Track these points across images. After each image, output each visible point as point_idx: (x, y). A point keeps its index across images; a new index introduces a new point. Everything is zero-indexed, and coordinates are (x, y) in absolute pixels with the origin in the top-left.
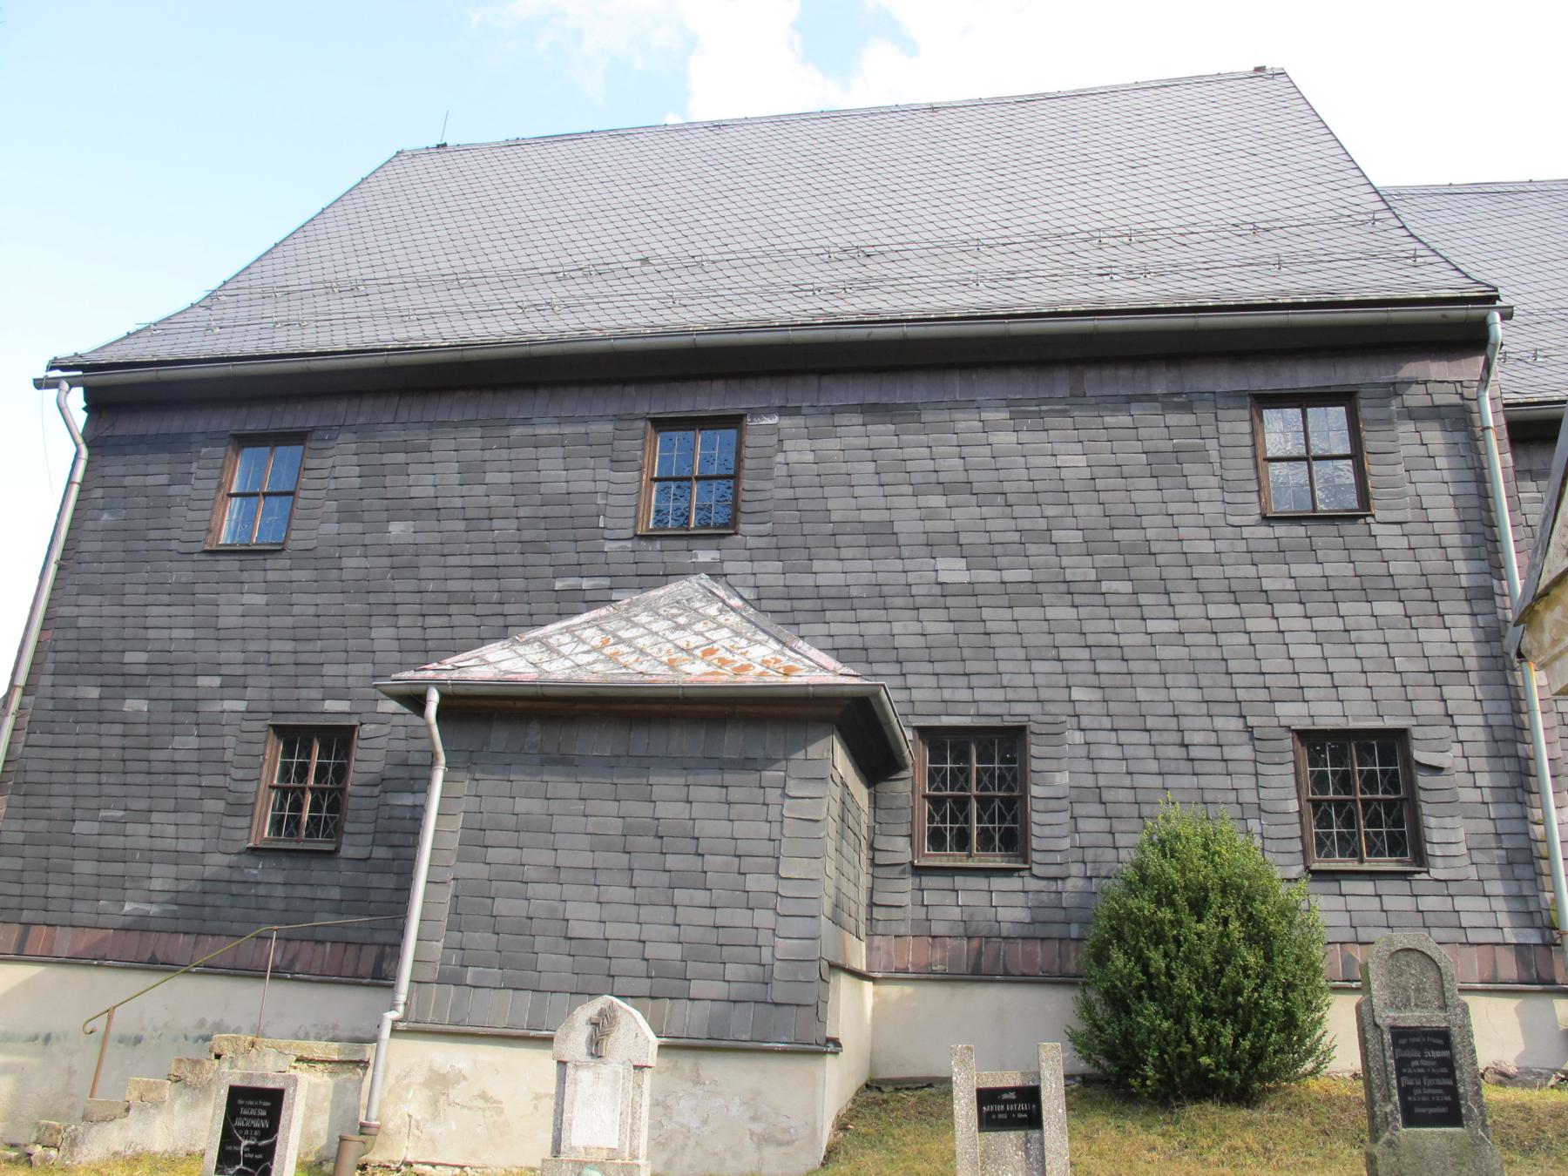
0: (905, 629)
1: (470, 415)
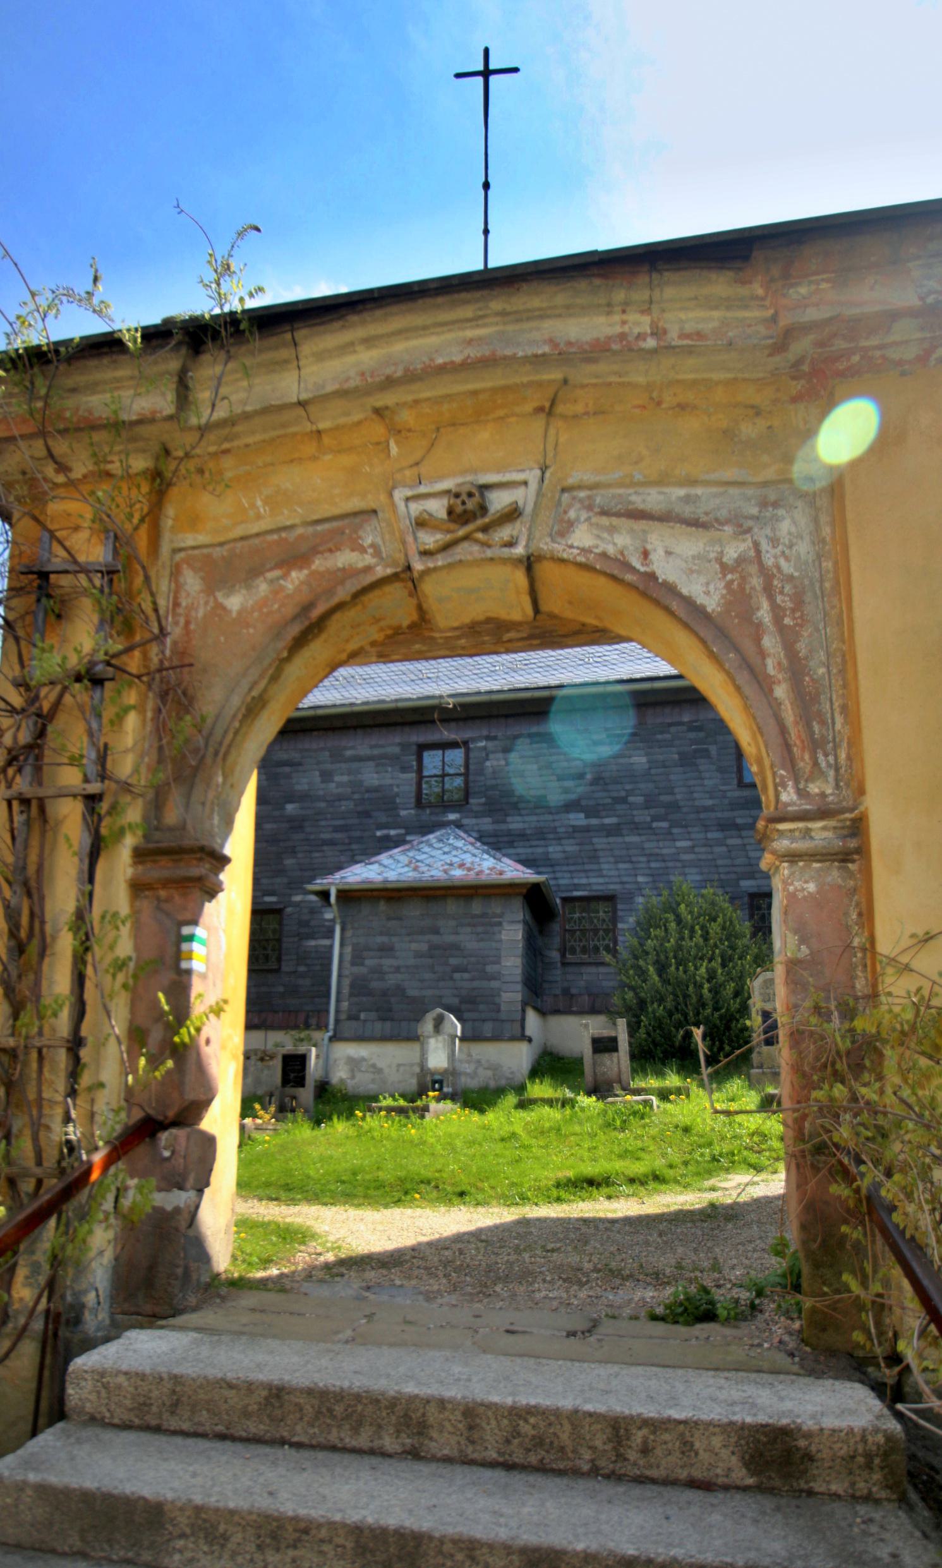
1: (322, 745)
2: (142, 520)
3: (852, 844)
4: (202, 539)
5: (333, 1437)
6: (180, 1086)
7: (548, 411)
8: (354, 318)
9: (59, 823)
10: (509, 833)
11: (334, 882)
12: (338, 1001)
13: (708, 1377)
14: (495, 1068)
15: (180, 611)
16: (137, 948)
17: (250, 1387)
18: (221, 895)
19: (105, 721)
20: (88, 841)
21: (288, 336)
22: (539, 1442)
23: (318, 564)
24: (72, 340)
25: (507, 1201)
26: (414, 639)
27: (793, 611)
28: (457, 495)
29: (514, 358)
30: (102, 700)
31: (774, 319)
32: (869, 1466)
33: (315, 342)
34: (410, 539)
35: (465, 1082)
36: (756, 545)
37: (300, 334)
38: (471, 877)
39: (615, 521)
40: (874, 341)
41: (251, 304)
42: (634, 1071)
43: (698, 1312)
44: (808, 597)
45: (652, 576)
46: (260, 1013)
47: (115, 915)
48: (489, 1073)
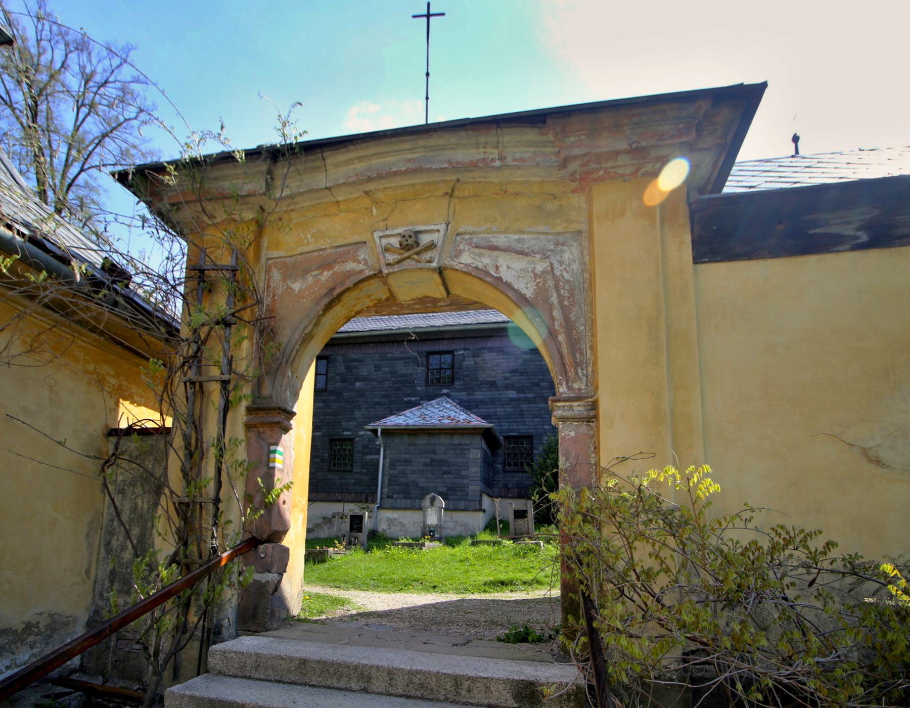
0: (500, 411)
2: (250, 244)
3: (592, 413)
4: (281, 253)
5: (329, 683)
6: (269, 523)
7: (451, 195)
8: (352, 147)
9: (210, 394)
10: (476, 401)
11: (379, 425)
12: (382, 488)
13: (508, 662)
14: (465, 526)
15: (271, 289)
16: (248, 456)
17: (291, 659)
18: (291, 431)
19: (232, 344)
20: (222, 403)
21: (320, 155)
22: (421, 686)
23: (337, 268)
24: (212, 155)
25: (457, 591)
26: (389, 305)
27: (569, 298)
28: (404, 237)
29: (430, 169)
30: (230, 334)
31: (559, 152)
32: (569, 700)
33: (334, 158)
34: (381, 257)
35: (446, 533)
36: (552, 264)
37: (326, 154)
38: (453, 425)
39: (482, 251)
40: (610, 164)
41: (300, 140)
42: (536, 529)
43: (522, 637)
44: (577, 292)
45: (500, 279)
46: (319, 489)
47: (236, 439)
48: (462, 528)
